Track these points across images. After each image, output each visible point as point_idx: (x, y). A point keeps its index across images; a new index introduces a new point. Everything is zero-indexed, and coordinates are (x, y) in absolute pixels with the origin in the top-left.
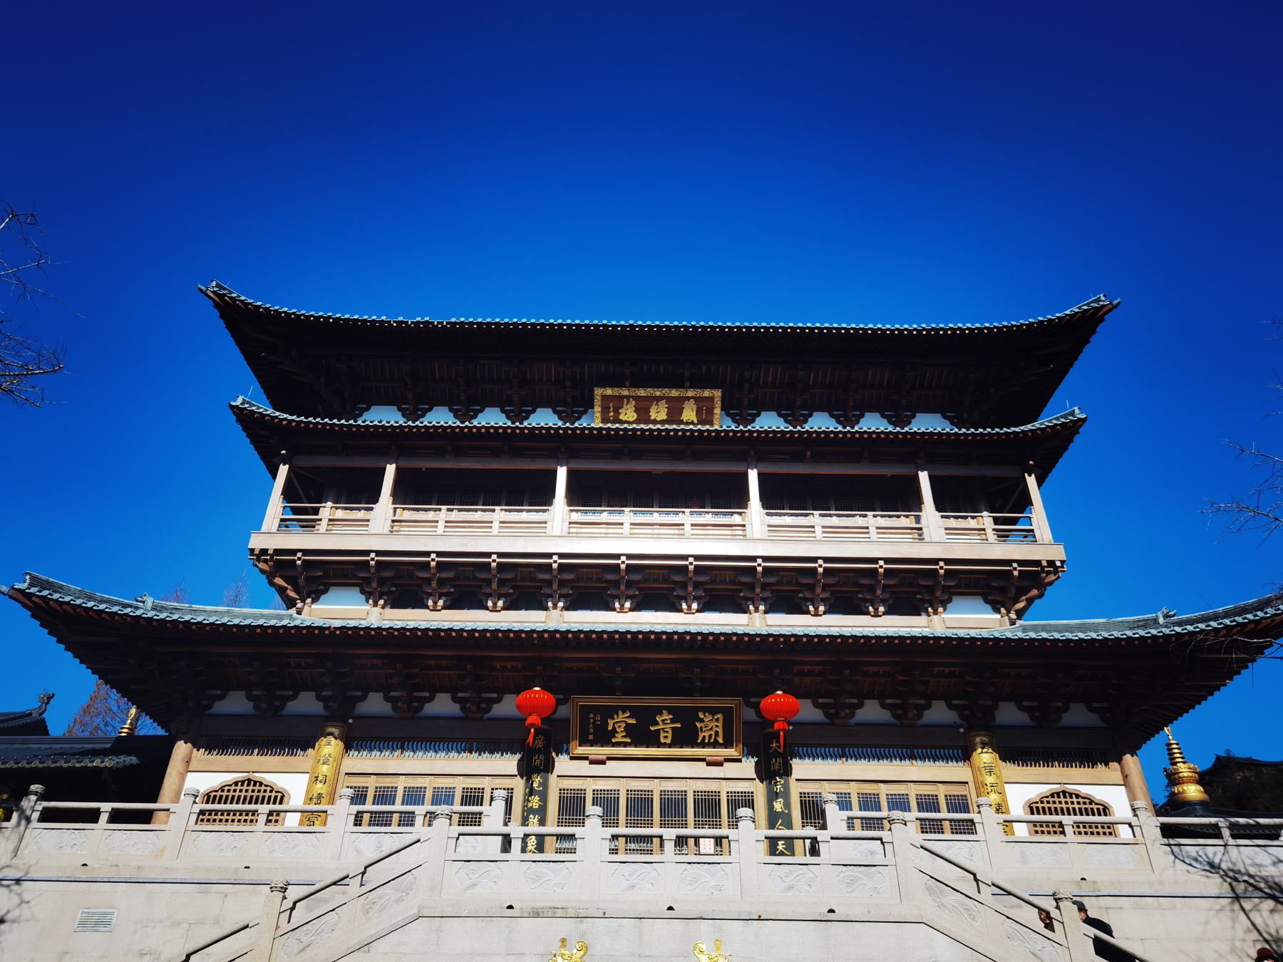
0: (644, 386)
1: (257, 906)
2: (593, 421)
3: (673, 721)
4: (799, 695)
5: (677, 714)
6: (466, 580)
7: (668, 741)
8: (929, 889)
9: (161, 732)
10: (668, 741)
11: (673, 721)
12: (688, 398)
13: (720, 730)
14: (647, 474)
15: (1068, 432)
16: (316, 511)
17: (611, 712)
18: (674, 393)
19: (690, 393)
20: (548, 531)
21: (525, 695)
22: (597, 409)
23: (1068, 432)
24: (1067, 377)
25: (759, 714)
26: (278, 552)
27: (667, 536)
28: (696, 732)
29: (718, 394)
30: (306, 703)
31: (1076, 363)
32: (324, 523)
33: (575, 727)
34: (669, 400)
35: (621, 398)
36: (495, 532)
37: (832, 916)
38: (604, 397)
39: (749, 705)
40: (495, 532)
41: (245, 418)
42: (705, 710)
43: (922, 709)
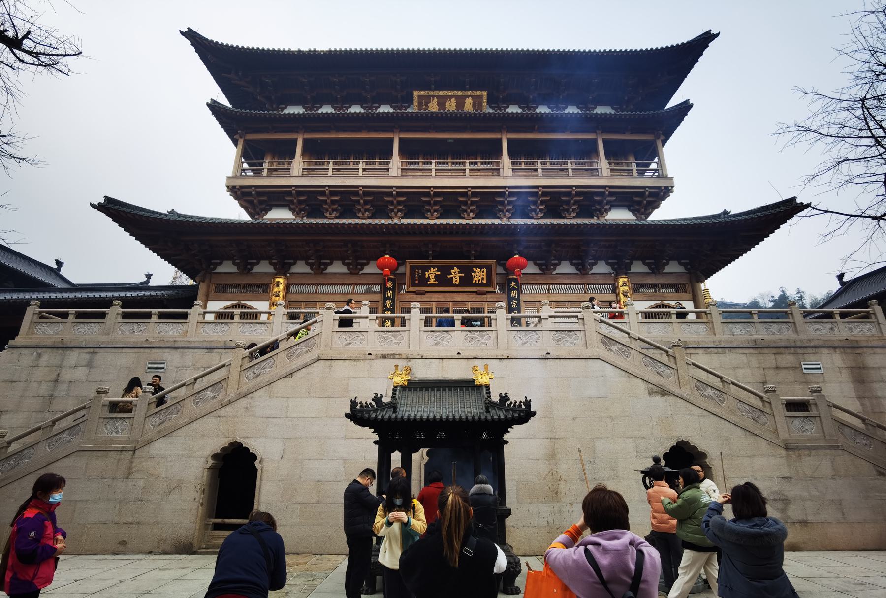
0: (442, 90)
1: (235, 358)
2: (413, 109)
3: (460, 272)
4: (528, 259)
5: (462, 269)
6: (347, 200)
7: (457, 283)
8: (603, 342)
9: (195, 283)
10: (457, 283)
11: (460, 272)
12: (468, 97)
13: (485, 277)
14: (445, 140)
15: (686, 107)
16: (261, 165)
17: (427, 268)
18: (460, 93)
19: (469, 93)
20: (390, 174)
21: (381, 260)
22: (416, 104)
23: (686, 107)
24: (697, 66)
25: (505, 269)
26: (242, 187)
27: (457, 177)
28: (472, 278)
29: (485, 93)
30: (264, 267)
31: (706, 52)
32: (265, 172)
33: (408, 278)
34: (457, 97)
35: (429, 97)
36: (360, 177)
37: (549, 356)
38: (419, 96)
39: (499, 264)
40: (360, 177)
41: (214, 107)
42: (476, 267)
43: (592, 265)
